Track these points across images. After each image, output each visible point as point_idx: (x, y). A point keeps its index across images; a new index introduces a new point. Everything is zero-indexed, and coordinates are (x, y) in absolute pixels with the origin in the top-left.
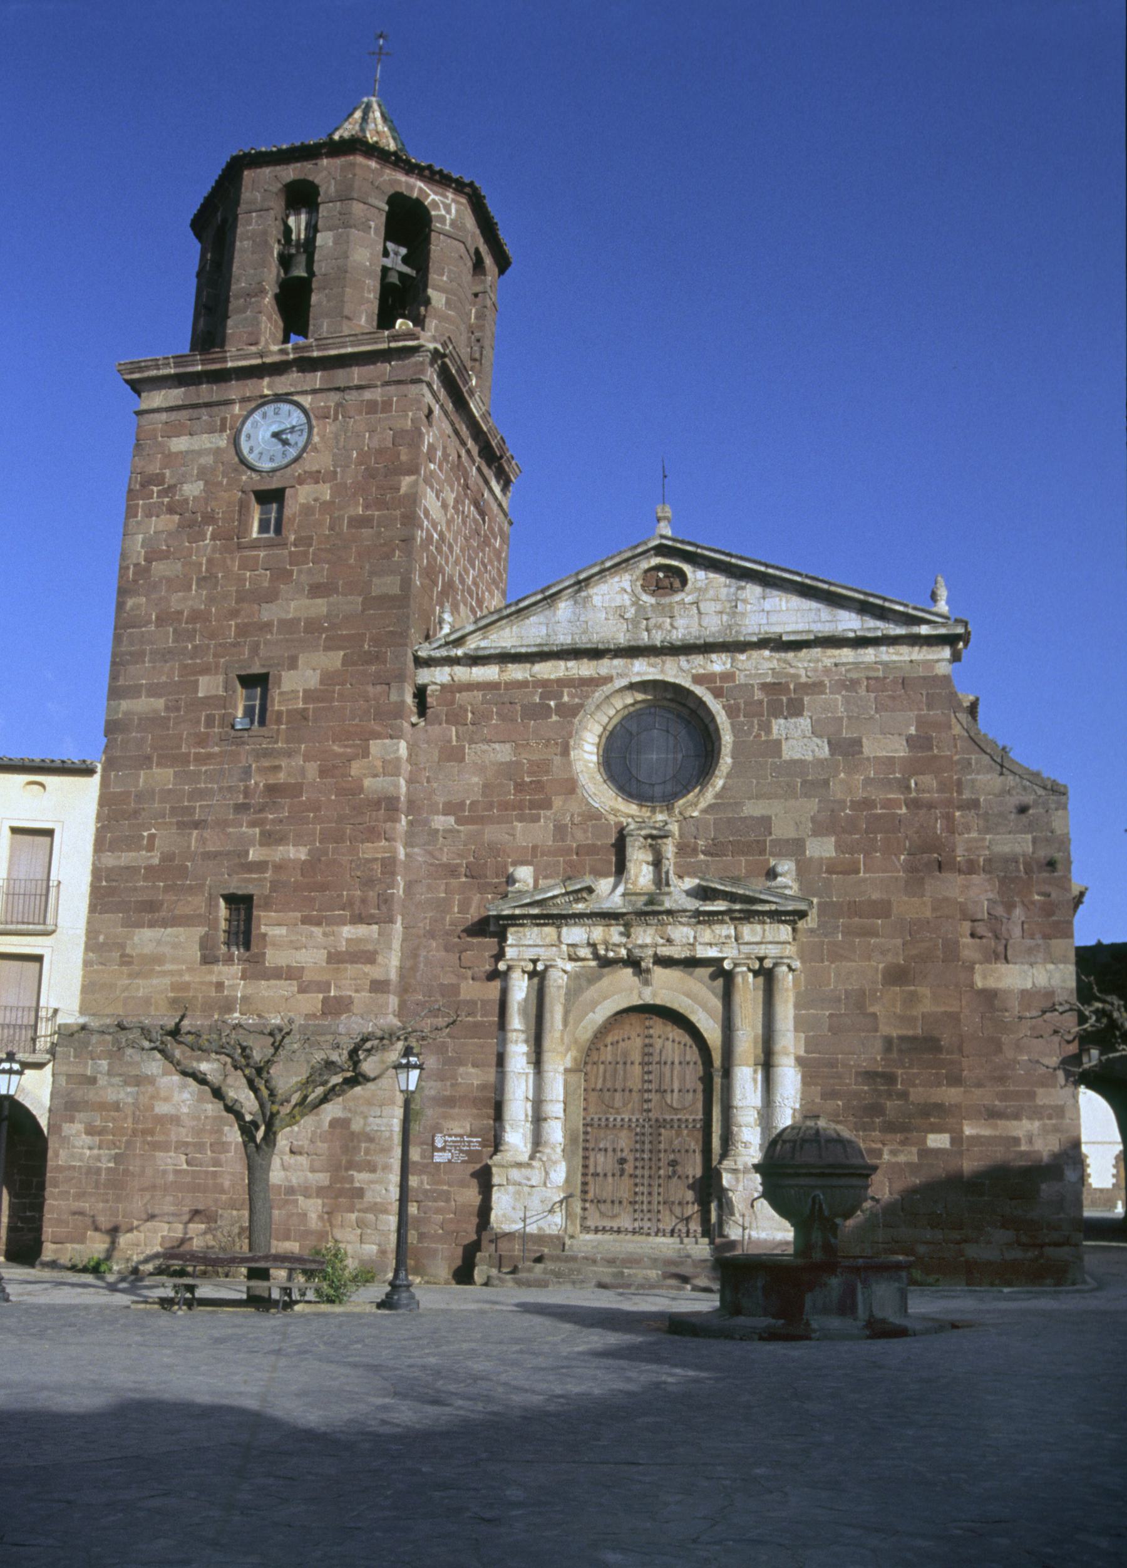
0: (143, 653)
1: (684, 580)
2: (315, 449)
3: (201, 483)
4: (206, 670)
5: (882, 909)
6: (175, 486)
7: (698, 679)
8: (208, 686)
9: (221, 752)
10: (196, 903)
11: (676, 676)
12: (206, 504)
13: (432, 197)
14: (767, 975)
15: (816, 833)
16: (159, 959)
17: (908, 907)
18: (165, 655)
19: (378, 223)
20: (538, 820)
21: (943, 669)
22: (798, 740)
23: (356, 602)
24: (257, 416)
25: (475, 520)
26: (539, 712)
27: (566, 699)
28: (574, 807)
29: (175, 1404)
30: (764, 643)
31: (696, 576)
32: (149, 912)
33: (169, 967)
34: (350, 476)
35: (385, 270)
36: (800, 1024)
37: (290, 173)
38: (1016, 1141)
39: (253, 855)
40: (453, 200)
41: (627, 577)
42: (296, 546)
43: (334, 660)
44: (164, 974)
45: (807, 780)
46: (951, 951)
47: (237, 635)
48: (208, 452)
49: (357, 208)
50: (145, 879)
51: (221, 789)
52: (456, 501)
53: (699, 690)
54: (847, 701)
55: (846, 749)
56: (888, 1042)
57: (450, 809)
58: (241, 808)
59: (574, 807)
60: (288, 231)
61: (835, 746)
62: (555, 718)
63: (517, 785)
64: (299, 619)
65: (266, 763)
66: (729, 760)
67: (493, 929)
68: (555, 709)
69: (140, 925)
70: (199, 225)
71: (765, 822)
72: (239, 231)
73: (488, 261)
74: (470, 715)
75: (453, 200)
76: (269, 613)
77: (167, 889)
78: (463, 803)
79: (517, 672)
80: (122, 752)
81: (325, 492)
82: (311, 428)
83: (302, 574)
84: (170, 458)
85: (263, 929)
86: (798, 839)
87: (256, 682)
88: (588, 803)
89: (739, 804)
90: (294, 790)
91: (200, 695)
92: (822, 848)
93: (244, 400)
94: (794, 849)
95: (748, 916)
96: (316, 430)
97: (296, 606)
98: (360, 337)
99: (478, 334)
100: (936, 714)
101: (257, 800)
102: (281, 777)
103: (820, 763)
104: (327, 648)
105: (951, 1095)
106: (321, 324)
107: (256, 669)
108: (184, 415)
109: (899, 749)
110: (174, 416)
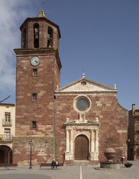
0: (20, 90)
1: (86, 84)
2: (41, 63)
4: (28, 93)
5: (108, 124)
7: (88, 96)
10: (29, 122)
14: (95, 131)
16: (25, 129)
17: (110, 124)
18: (23, 90)
19: (47, 31)
22: (99, 104)
23: (47, 85)
24: (33, 58)
26: (69, 99)
28: (73, 111)
29: (74, 152)
32: (23, 123)
33: (26, 130)
34: (45, 67)
38: (121, 149)
43: (45, 92)
45: (100, 109)
46: (115, 128)
50: (22, 119)
53: (88, 97)
55: (104, 105)
56: (108, 139)
60: (35, 31)
65: (37, 105)
67: (64, 127)
69: (22, 125)
70: (21, 28)
72: (29, 30)
76: (36, 85)
80: (18, 103)
81: (42, 69)
83: (40, 81)
84: (22, 63)
89: (92, 111)
92: (101, 117)
93: (31, 56)
94: (98, 117)
97: (40, 85)
101: (36, 109)
102: (39, 107)
104: (44, 90)
106: (41, 46)
107: (35, 93)
108: (23, 57)
109: (110, 105)
110: (21, 57)
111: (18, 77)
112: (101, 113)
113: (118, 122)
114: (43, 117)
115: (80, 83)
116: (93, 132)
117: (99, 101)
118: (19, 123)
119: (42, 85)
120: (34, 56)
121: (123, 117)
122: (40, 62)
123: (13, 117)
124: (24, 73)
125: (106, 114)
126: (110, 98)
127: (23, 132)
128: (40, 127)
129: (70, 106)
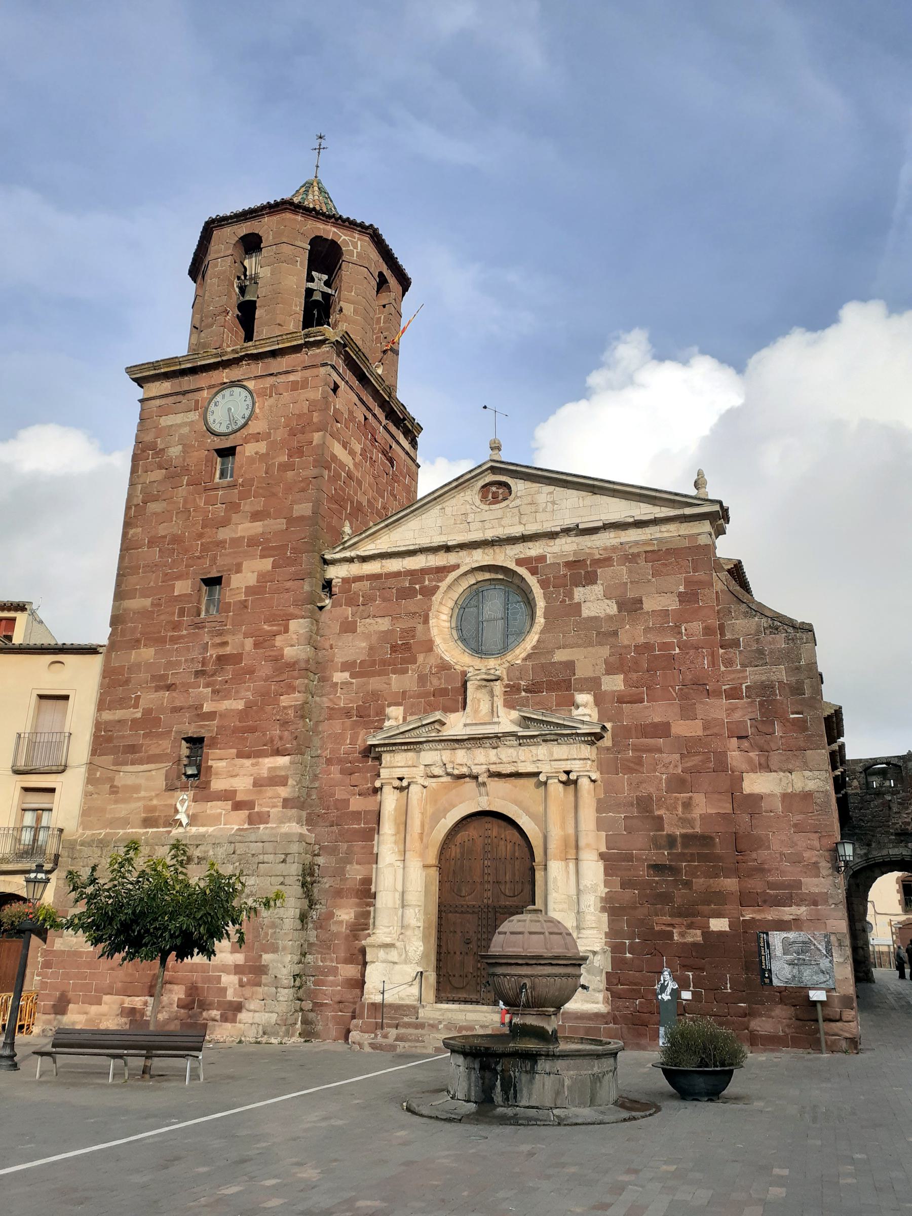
3: (180, 447)
4: (179, 577)
5: (662, 730)
6: (164, 449)
7: (519, 562)
8: (182, 587)
9: (189, 634)
10: (166, 745)
11: (504, 561)
12: (184, 460)
13: (344, 237)
15: (609, 672)
16: (136, 788)
17: (683, 728)
18: (153, 567)
20: (407, 672)
21: (703, 540)
22: (594, 602)
24: (219, 398)
25: (383, 463)
26: (406, 594)
27: (427, 583)
30: (567, 531)
31: (519, 486)
32: (131, 753)
34: (280, 435)
35: (309, 292)
36: (600, 825)
37: (243, 229)
39: (206, 708)
40: (359, 239)
41: (469, 492)
42: (243, 486)
43: (267, 564)
44: (139, 799)
45: (601, 632)
47: (201, 551)
48: (185, 424)
49: (286, 249)
51: (186, 660)
52: (364, 450)
53: (522, 571)
54: (630, 571)
56: (671, 841)
57: (346, 666)
58: (198, 674)
59: (432, 661)
61: (621, 606)
62: (419, 597)
63: (392, 647)
64: (244, 537)
65: (218, 640)
66: (542, 620)
67: (372, 754)
68: (415, 589)
69: (125, 763)
71: (570, 666)
73: (392, 281)
74: (361, 599)
75: (359, 239)
76: (224, 534)
77: (145, 736)
78: (355, 661)
79: (394, 565)
82: (254, 404)
83: (247, 506)
85: (210, 763)
86: (595, 678)
87: (213, 582)
88: (441, 658)
89: (551, 652)
90: (235, 659)
91: (175, 594)
92: (615, 683)
93: (210, 387)
94: (592, 685)
95: (557, 738)
96: (257, 405)
97: (245, 528)
98: (284, 337)
99: (385, 334)
100: (700, 575)
101: (210, 667)
102: (228, 650)
103: (610, 618)
105: (730, 884)
106: (262, 330)
107: (214, 574)
108: (171, 400)
109: (672, 604)
111: (135, 502)
112: (612, 659)
113: (744, 713)
114: (249, 706)
115: (472, 495)
116: (555, 788)
117: (269, 768)
118: (115, 751)
119: (257, 527)
120: (224, 386)
121: (780, 674)
122: (253, 411)
123: (80, 720)
124: (167, 477)
125: (647, 668)
126: (661, 557)
127: (122, 810)
128: (231, 772)
129: (413, 629)
